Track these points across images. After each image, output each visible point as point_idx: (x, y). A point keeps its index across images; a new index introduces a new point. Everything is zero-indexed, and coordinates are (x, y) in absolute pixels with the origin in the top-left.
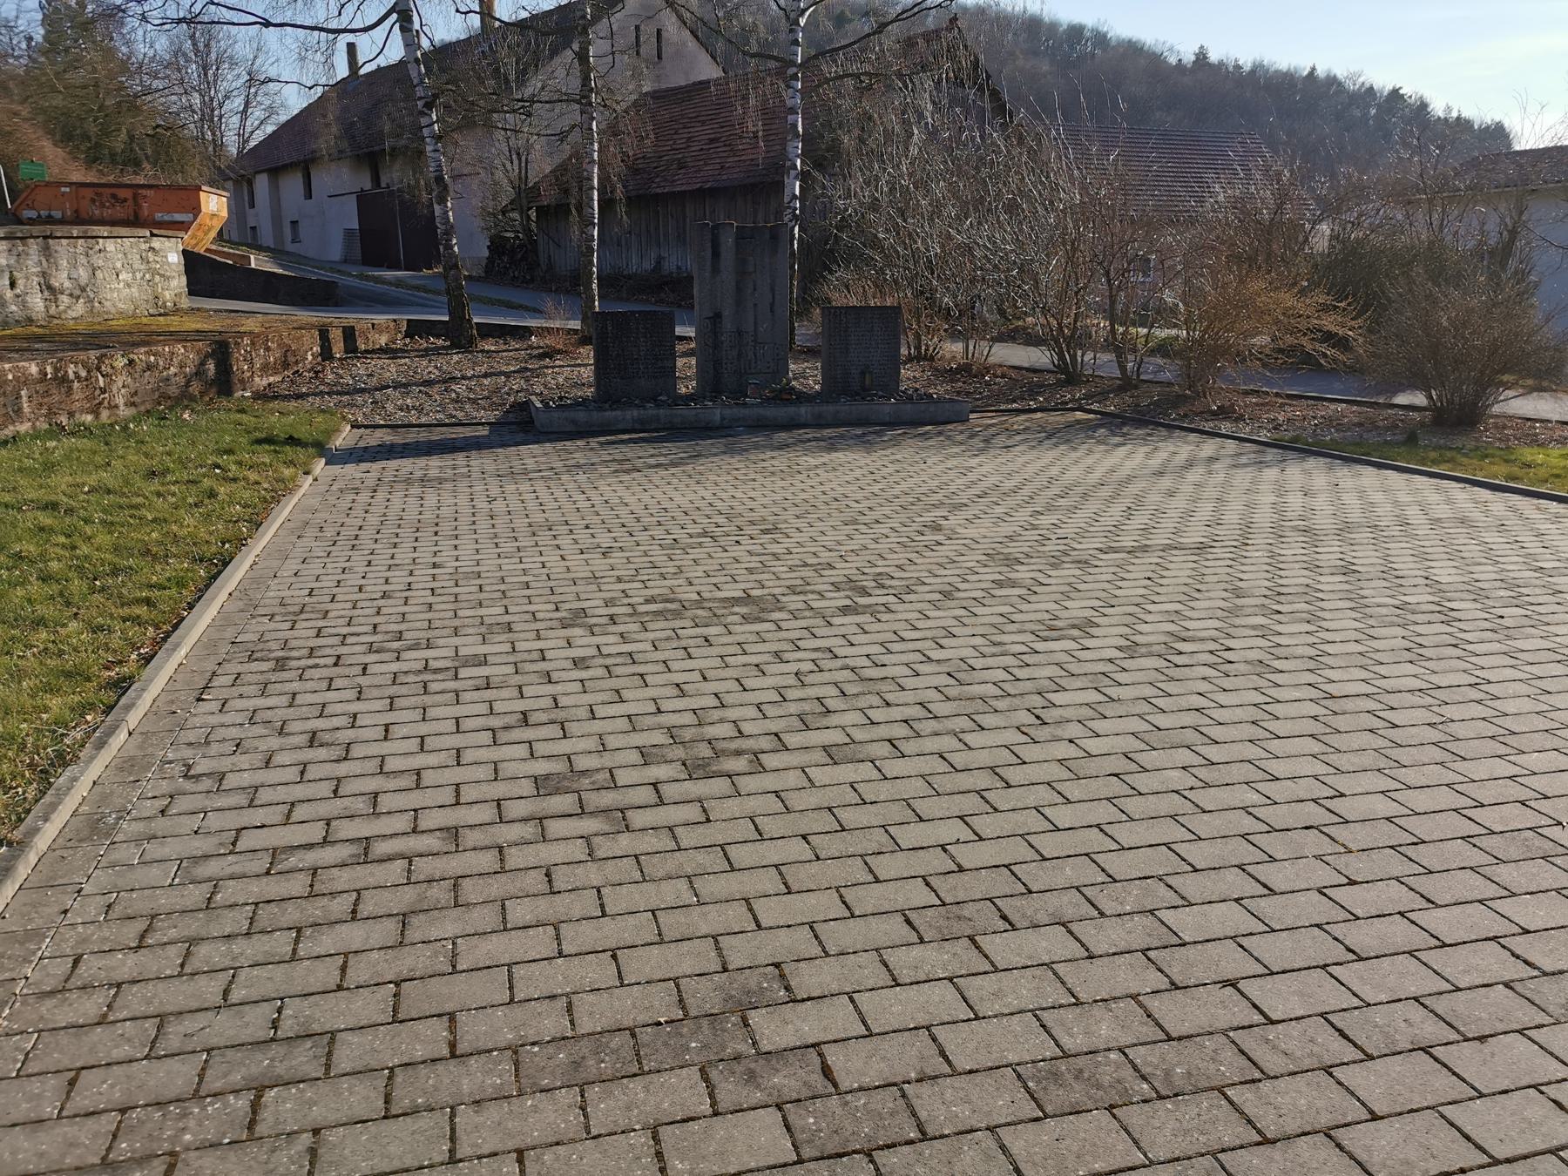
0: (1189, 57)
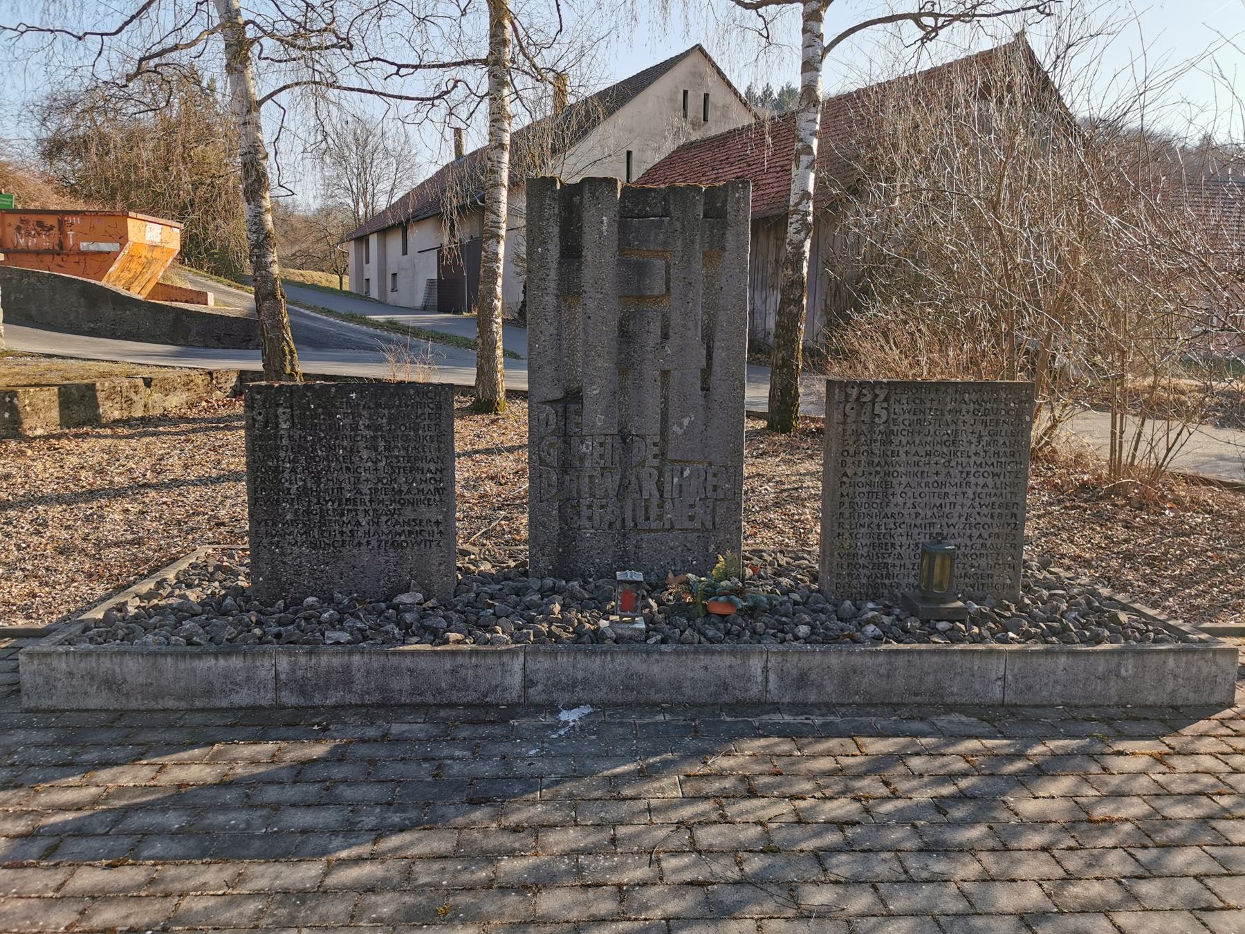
0: (1194, 141)
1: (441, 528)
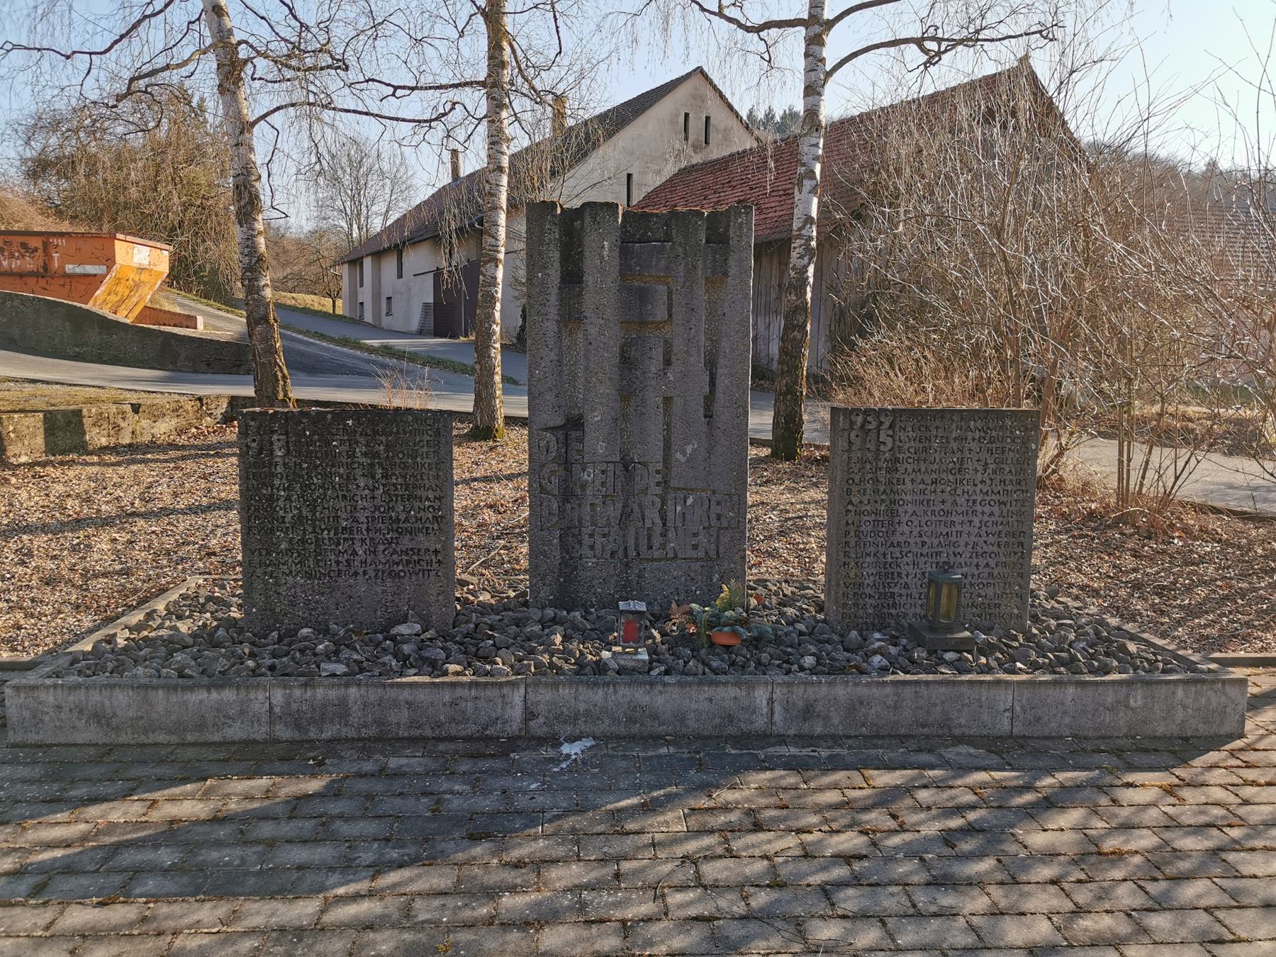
0: (1199, 166)
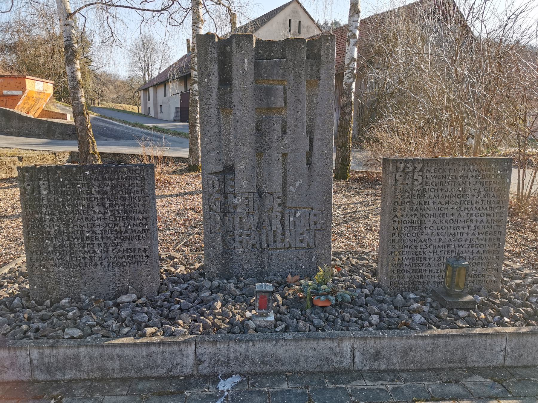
1: (147, 254)
